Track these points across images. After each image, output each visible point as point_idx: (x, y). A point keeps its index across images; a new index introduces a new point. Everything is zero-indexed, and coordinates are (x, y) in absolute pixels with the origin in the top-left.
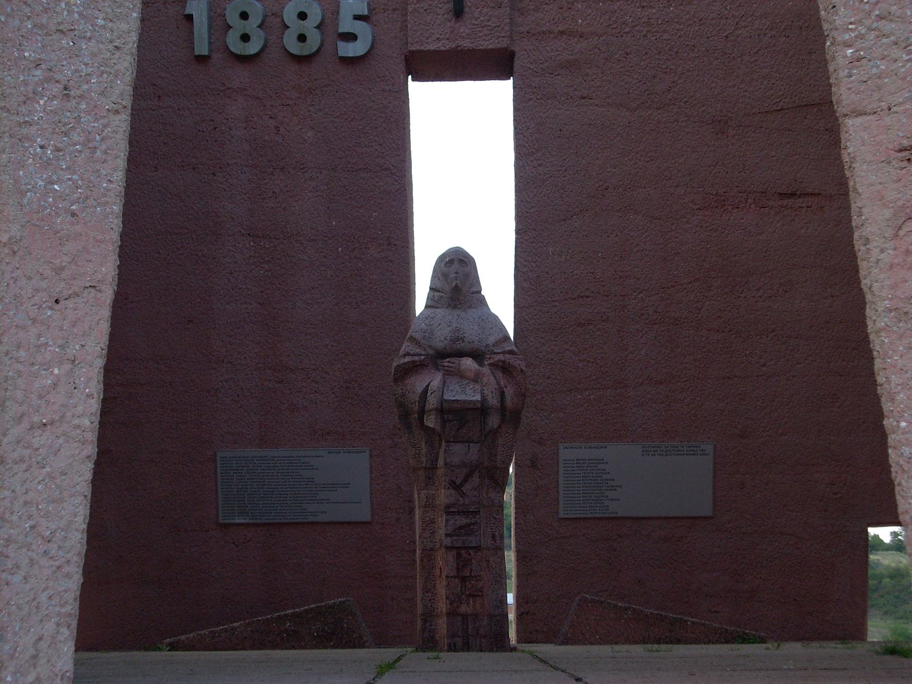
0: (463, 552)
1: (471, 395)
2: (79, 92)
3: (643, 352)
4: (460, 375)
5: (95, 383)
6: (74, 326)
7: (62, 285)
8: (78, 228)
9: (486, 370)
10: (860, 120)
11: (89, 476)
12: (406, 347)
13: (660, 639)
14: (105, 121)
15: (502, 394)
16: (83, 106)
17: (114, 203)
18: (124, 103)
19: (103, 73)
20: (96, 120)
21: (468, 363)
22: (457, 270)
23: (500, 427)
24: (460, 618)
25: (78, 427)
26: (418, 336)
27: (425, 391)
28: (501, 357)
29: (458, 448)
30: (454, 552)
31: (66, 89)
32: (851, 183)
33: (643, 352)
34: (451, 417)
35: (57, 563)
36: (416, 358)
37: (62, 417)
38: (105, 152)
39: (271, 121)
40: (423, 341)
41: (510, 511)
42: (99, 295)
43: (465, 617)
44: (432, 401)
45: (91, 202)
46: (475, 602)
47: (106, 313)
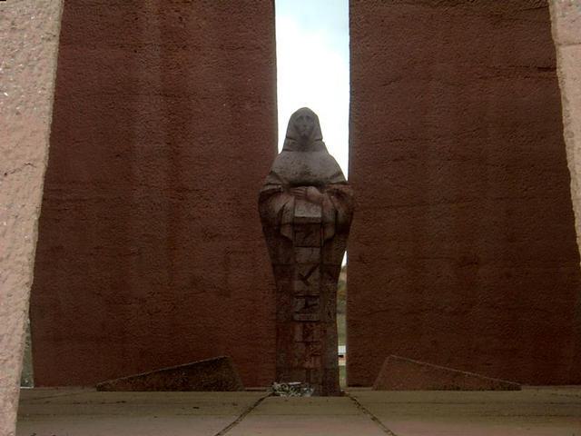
0: (307, 324)
1: (314, 213)
2: (23, 26)
3: (440, 180)
4: (307, 199)
5: (32, 231)
6: (17, 191)
7: (10, 163)
8: (21, 123)
9: (325, 195)
10: (568, 48)
11: (27, 297)
12: (269, 179)
13: (445, 387)
14: (41, 46)
15: (337, 213)
16: (25, 36)
17: (46, 105)
18: (54, 34)
19: (39, 12)
20: (34, 46)
21: (313, 190)
22: (306, 126)
23: (334, 236)
24: (305, 371)
25: (19, 262)
26: (277, 171)
27: (282, 211)
28: (336, 186)
30: (301, 325)
31: (13, 24)
32: (562, 93)
33: (440, 180)
34: (299, 229)
35: (5, 358)
36: (275, 187)
37: (9, 256)
38: (40, 69)
39: (176, 13)
40: (280, 175)
41: (342, 289)
42: (35, 170)
44: (287, 218)
45: (30, 104)
46: (315, 360)
47: (40, 182)
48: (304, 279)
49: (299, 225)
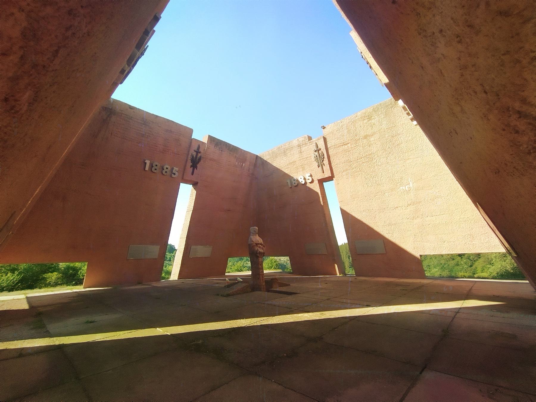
4: (259, 247)
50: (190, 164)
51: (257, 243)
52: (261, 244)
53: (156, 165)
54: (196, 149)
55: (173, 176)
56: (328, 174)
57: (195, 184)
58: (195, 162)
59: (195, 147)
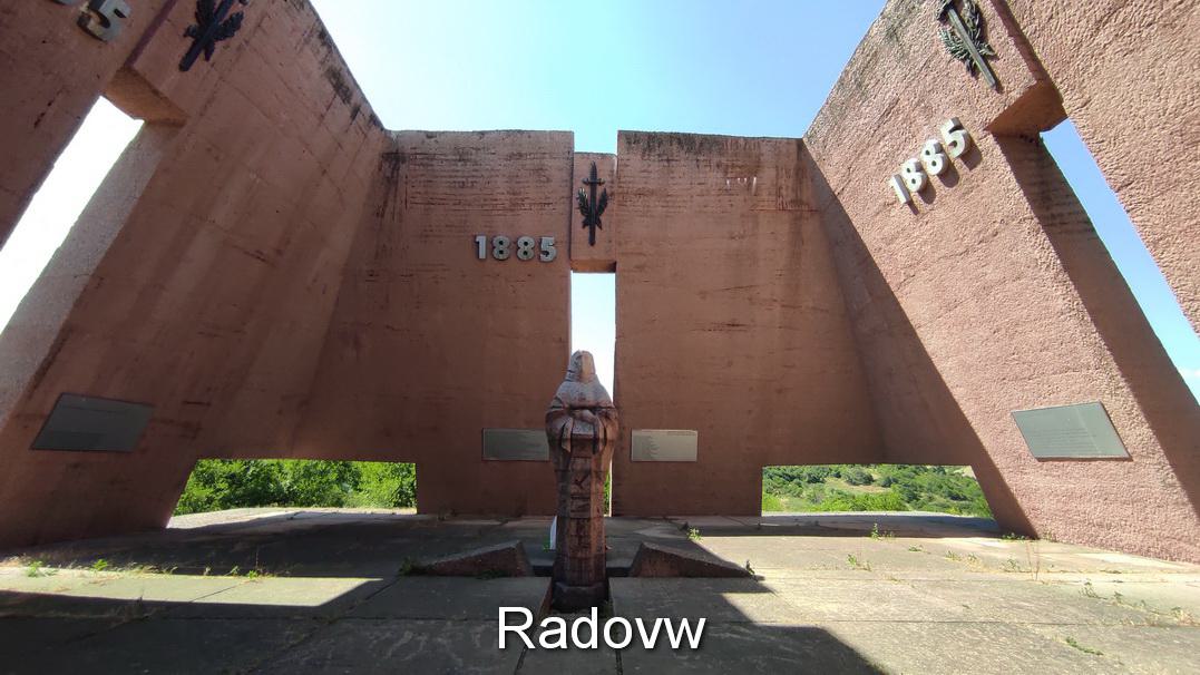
4: (582, 419)
21: (587, 413)
29: (579, 461)
43: (580, 560)
44: (567, 435)
48: (577, 483)
49: (576, 440)
50: (578, 218)
51: (576, 403)
52: (593, 409)
53: (501, 243)
54: (587, 175)
55: (543, 257)
56: (1018, 78)
57: (612, 268)
58: (593, 212)
59: (583, 172)
